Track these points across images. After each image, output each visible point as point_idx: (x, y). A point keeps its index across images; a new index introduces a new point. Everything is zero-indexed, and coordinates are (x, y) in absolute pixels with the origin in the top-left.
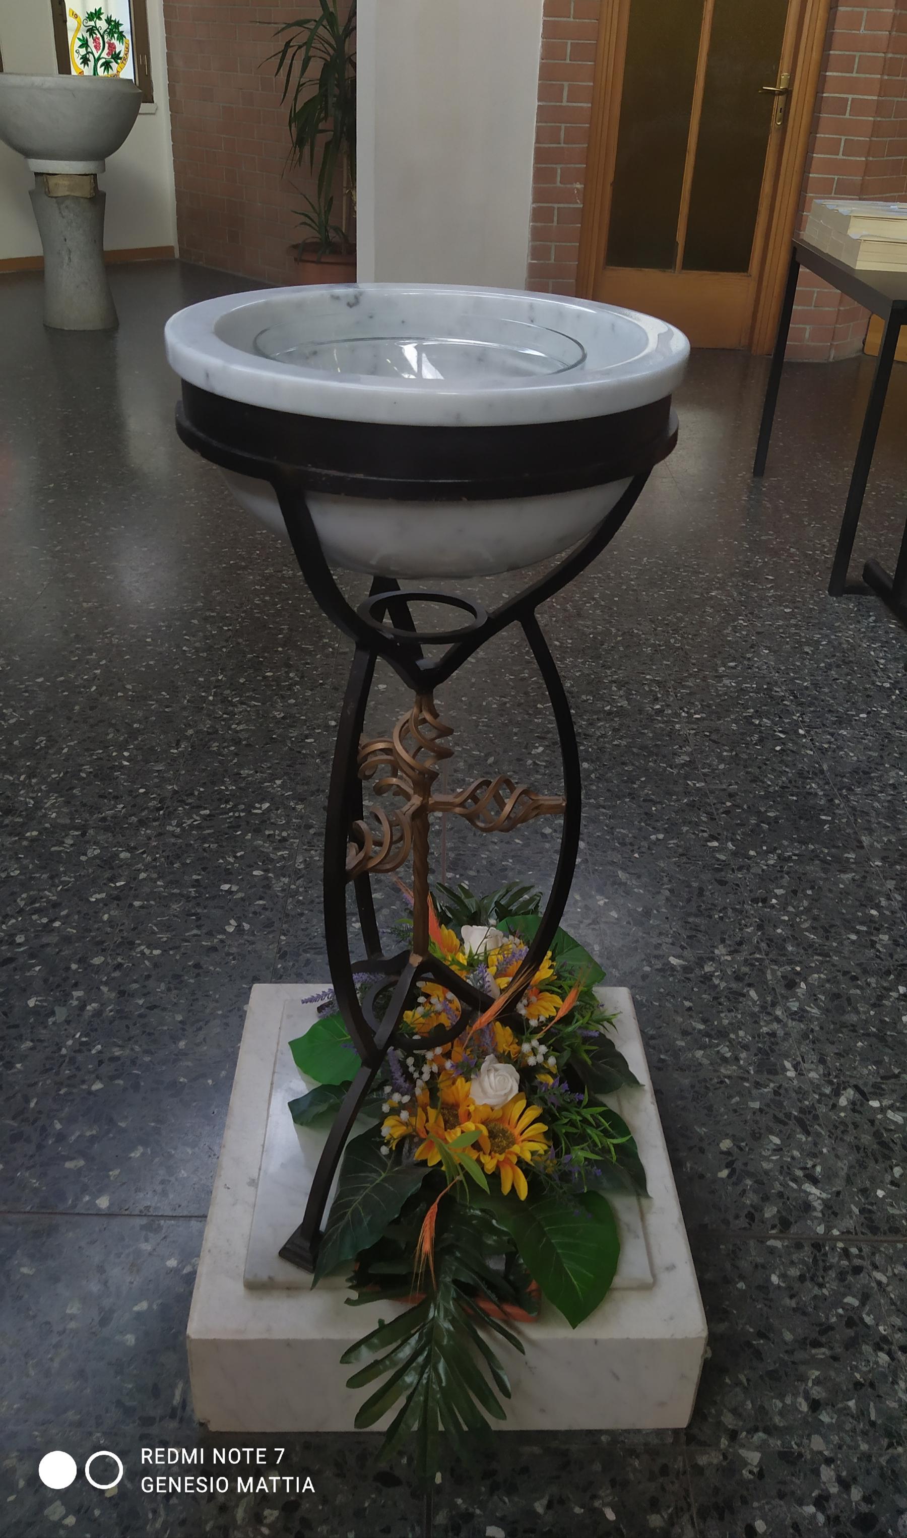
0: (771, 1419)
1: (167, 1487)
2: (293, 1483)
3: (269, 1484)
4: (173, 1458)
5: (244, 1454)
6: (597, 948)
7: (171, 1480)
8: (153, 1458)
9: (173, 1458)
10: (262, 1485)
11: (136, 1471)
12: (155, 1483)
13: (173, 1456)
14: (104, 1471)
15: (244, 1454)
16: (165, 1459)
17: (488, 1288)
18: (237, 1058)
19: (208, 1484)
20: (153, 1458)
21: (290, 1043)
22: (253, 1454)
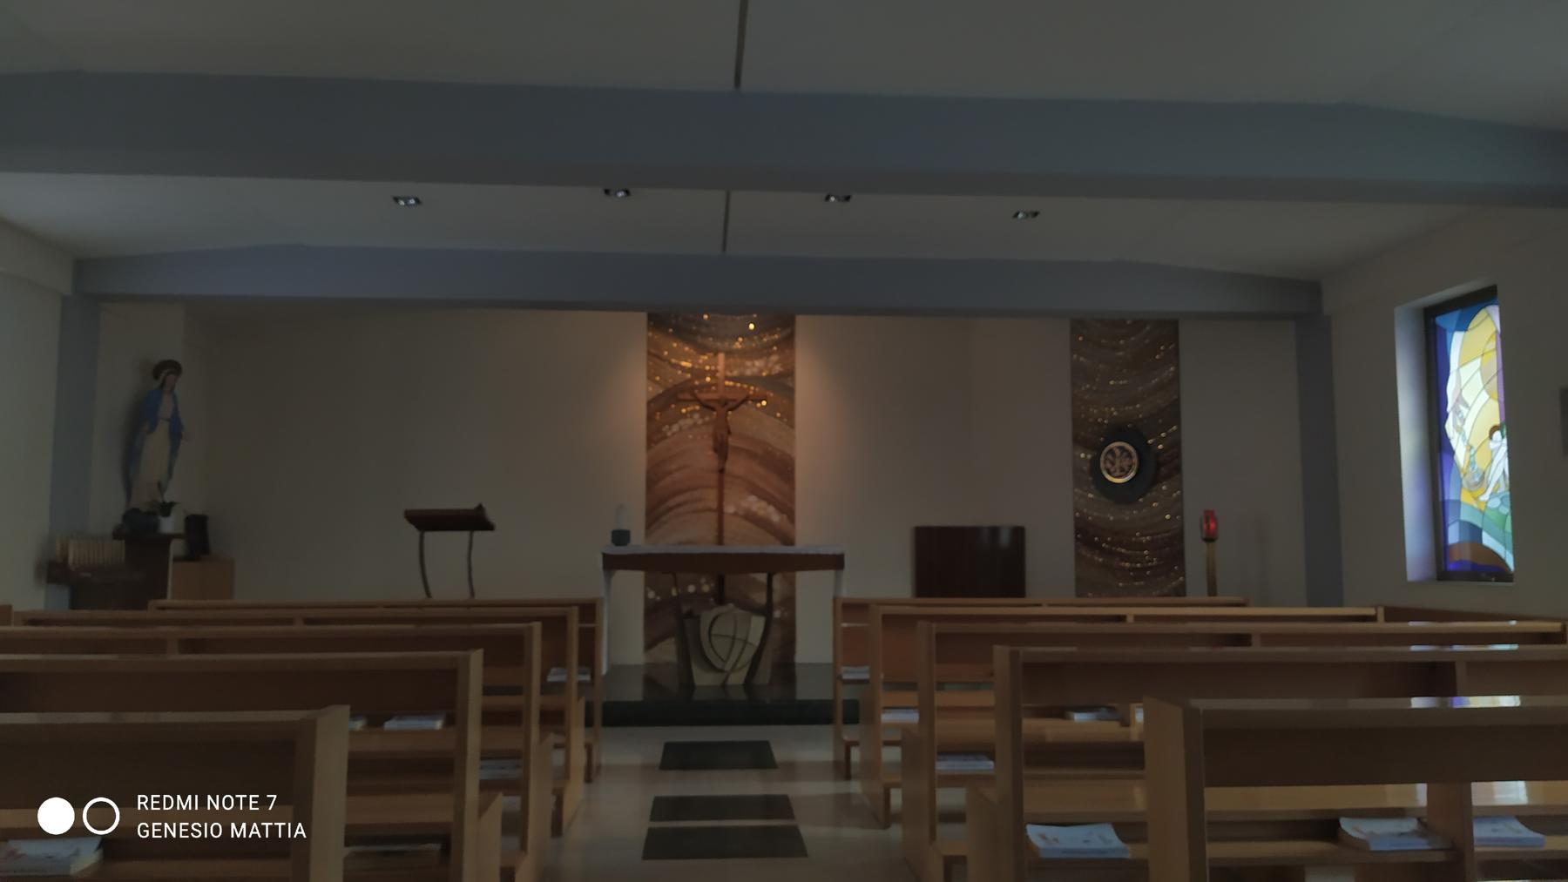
1: (162, 833)
2: (285, 829)
3: (262, 829)
4: (168, 804)
5: (237, 800)
8: (149, 804)
9: (168, 804)
10: (255, 831)
15: (237, 800)
16: (160, 805)
20: (149, 804)
22: (246, 801)
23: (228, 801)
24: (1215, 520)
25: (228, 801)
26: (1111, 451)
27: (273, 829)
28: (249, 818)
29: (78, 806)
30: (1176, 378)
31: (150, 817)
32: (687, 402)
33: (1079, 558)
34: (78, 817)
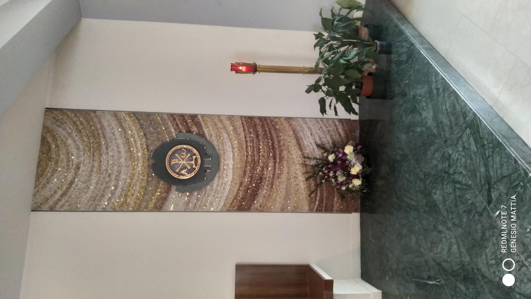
0: (414, 110)
1: (514, 244)
2: (513, 203)
3: (513, 210)
4: (505, 242)
5: (503, 219)
6: (335, 199)
7: (512, 243)
8: (505, 249)
9: (505, 242)
10: (514, 213)
11: (509, 254)
12: (513, 248)
13: (503, 242)
14: (508, 265)
15: (503, 219)
16: (505, 245)
17: (319, 200)
18: (161, 22)
19: (513, 230)
20: (505, 249)
21: (240, 268)
22: (503, 216)
23: (503, 222)
24: (240, 64)
25: (503, 222)
26: (189, 172)
27: (513, 206)
28: (509, 215)
29: (504, 273)
30: (115, 114)
31: (509, 248)
32: (198, 128)
33: (263, 209)
34: (510, 272)
